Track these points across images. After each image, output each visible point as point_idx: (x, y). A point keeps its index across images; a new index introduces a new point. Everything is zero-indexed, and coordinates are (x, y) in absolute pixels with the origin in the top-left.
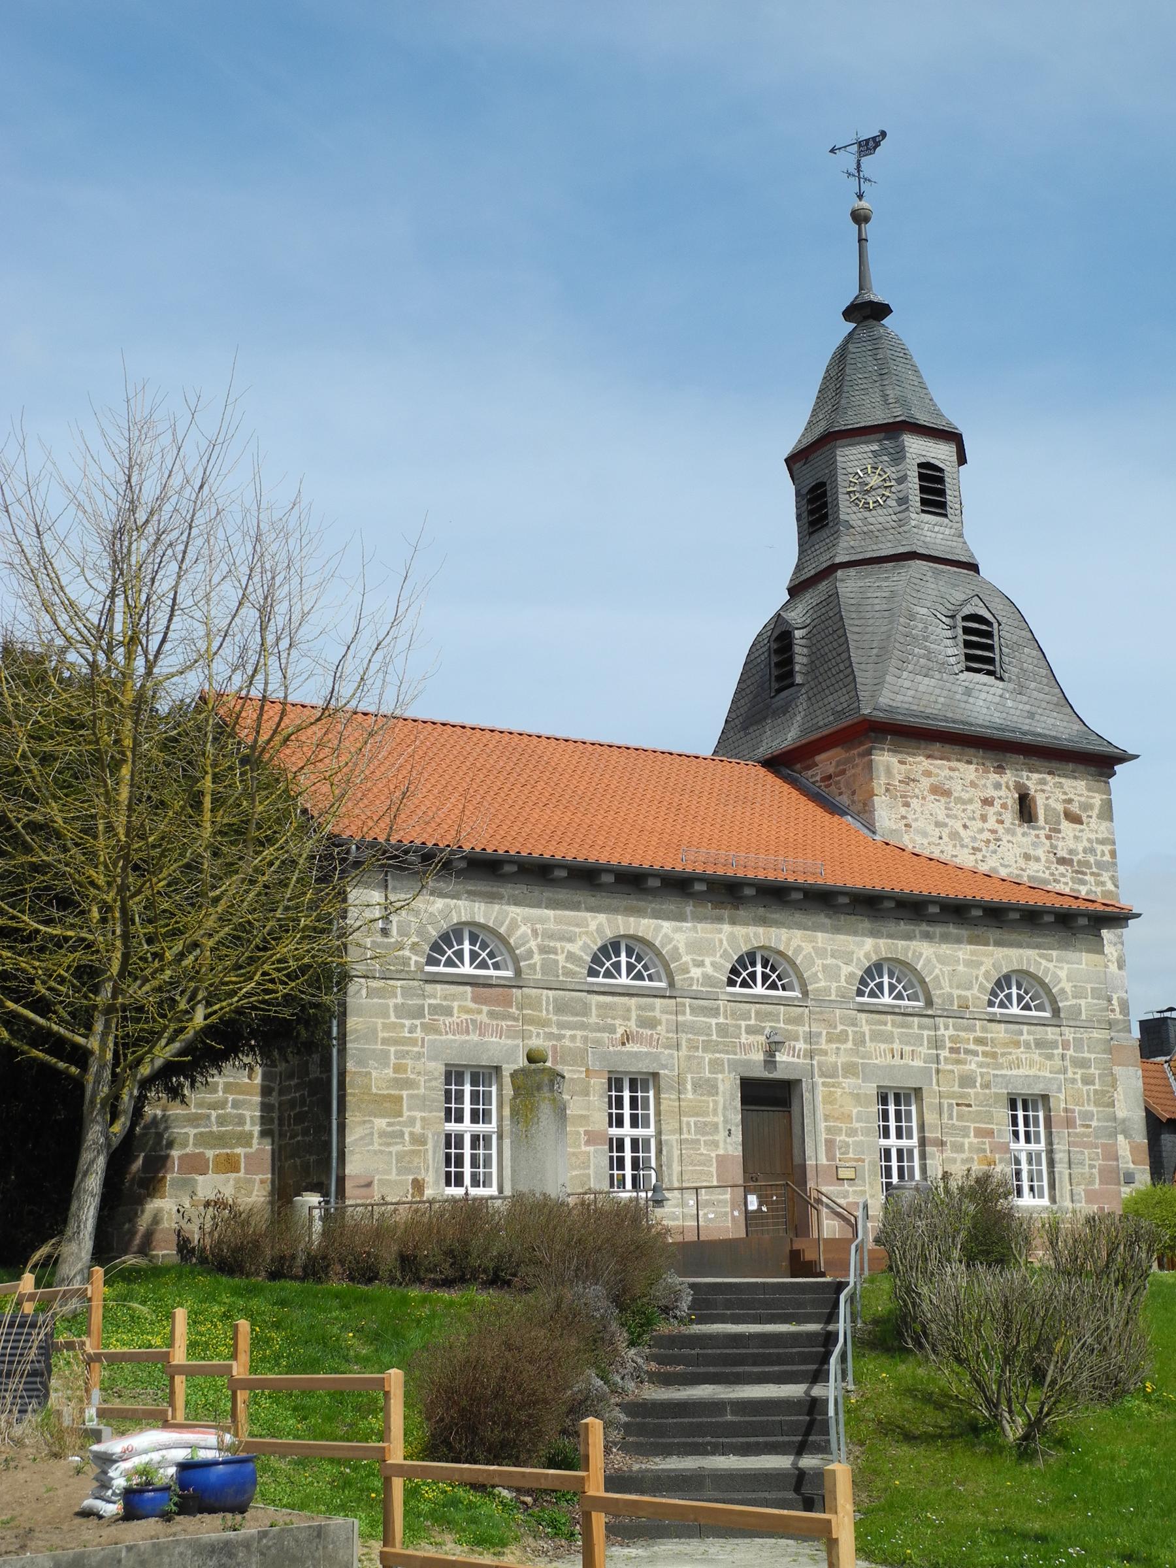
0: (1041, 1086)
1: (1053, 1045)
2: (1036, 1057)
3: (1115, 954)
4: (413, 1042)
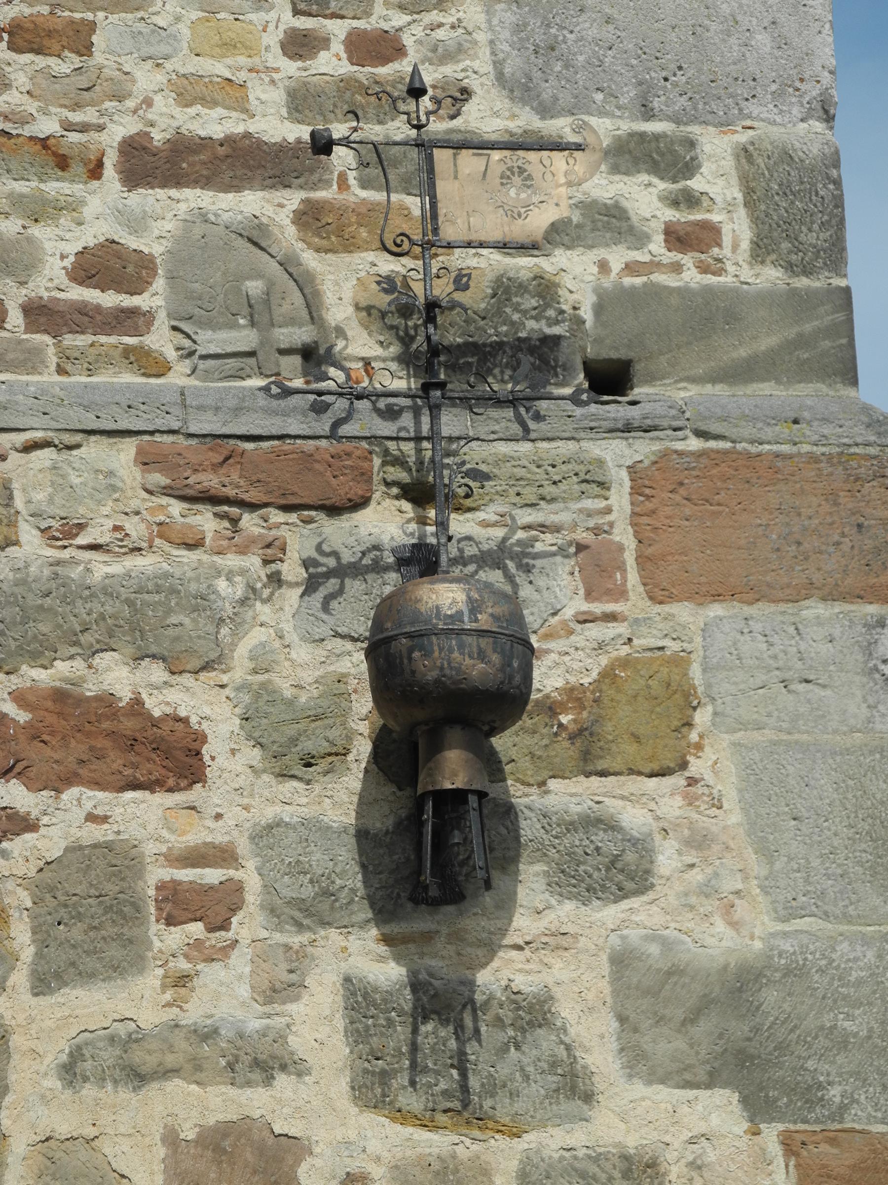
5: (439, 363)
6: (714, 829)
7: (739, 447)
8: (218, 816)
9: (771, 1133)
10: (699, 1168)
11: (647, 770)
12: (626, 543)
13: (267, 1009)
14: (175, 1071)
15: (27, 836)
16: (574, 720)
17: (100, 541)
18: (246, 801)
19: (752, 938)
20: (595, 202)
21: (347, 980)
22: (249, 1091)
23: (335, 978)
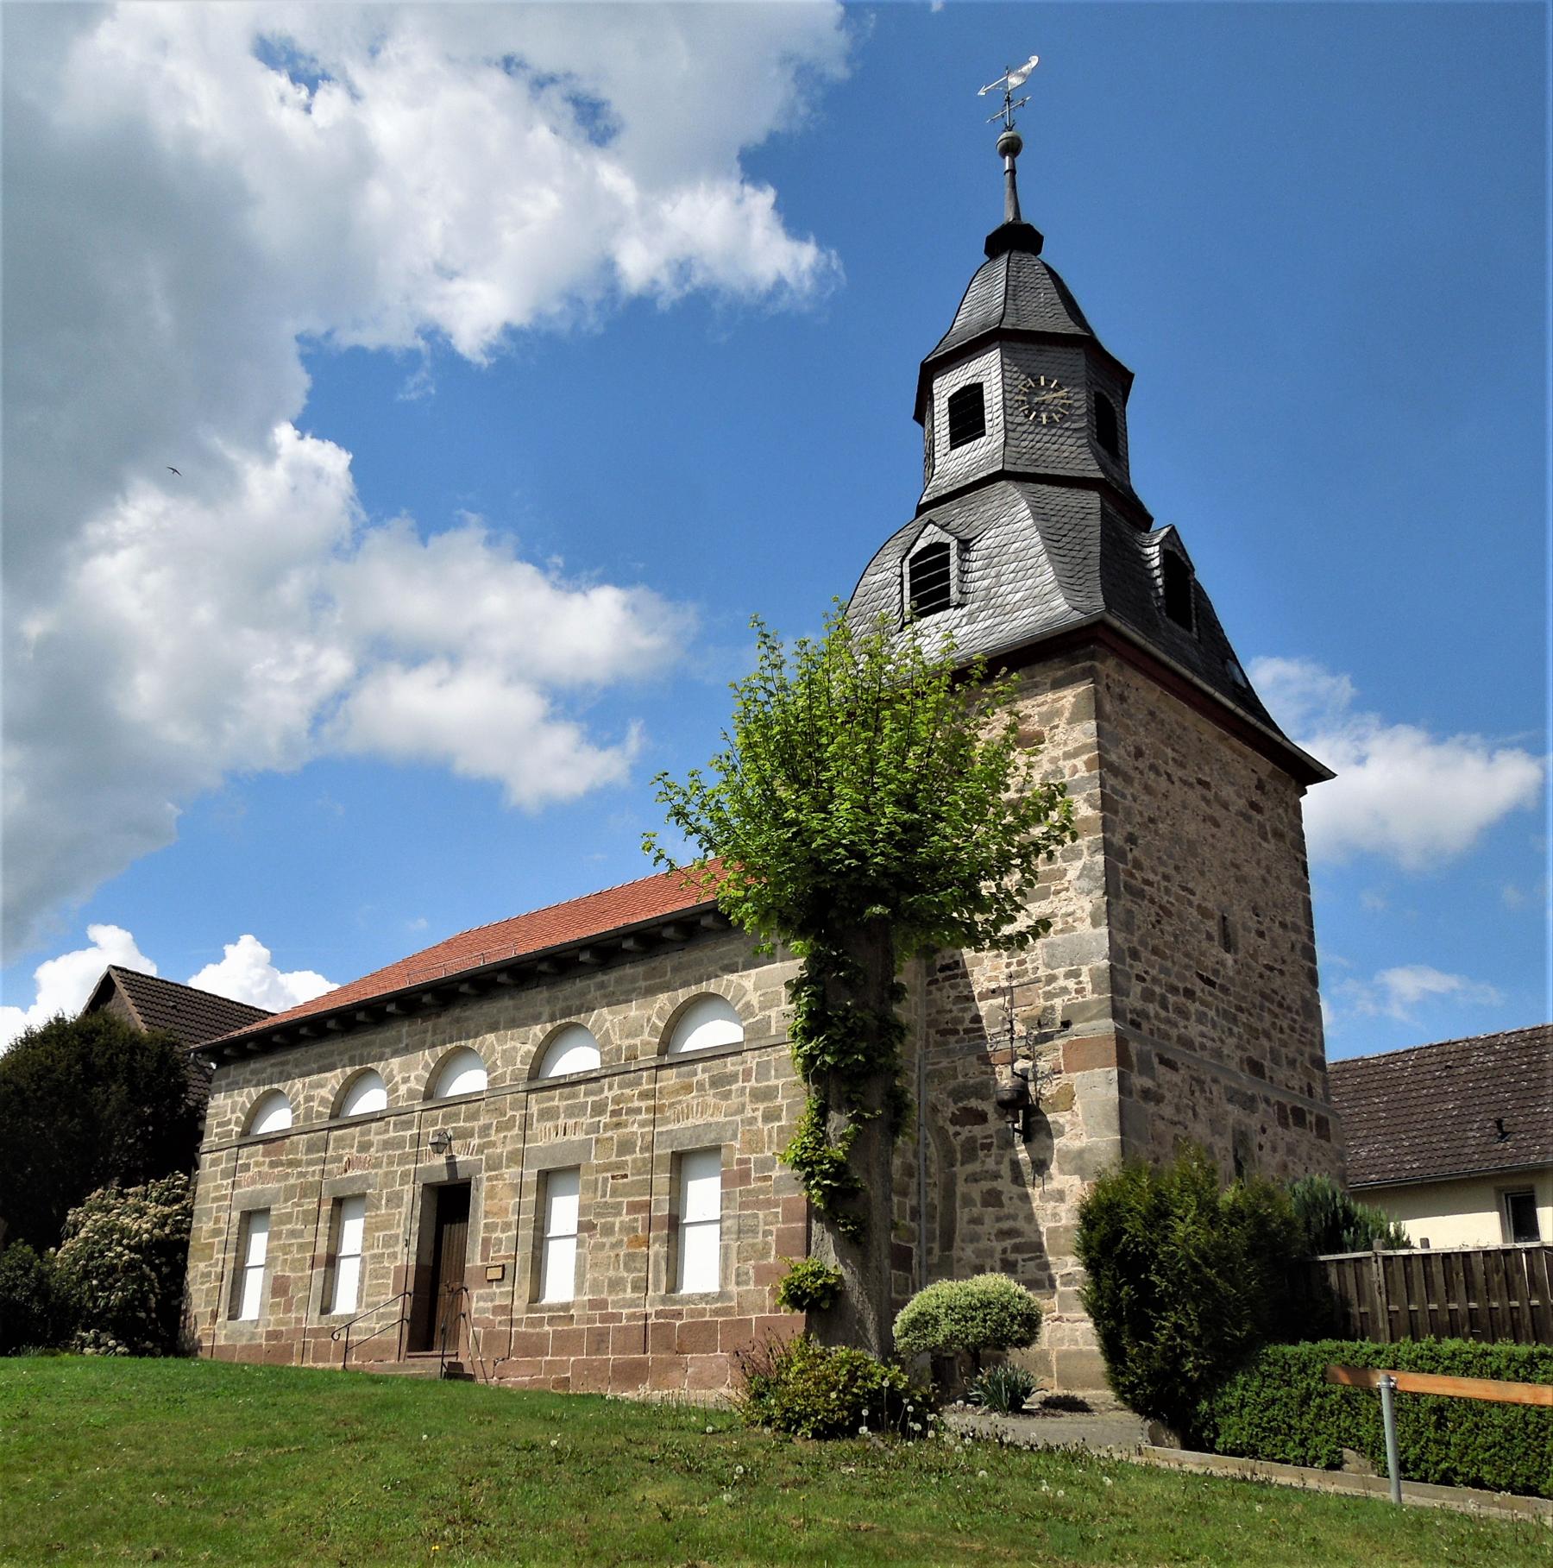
0: (712, 1136)
1: (733, 1078)
2: (711, 1100)
3: (1088, 907)
4: (224, 1197)
5: (95, 1306)
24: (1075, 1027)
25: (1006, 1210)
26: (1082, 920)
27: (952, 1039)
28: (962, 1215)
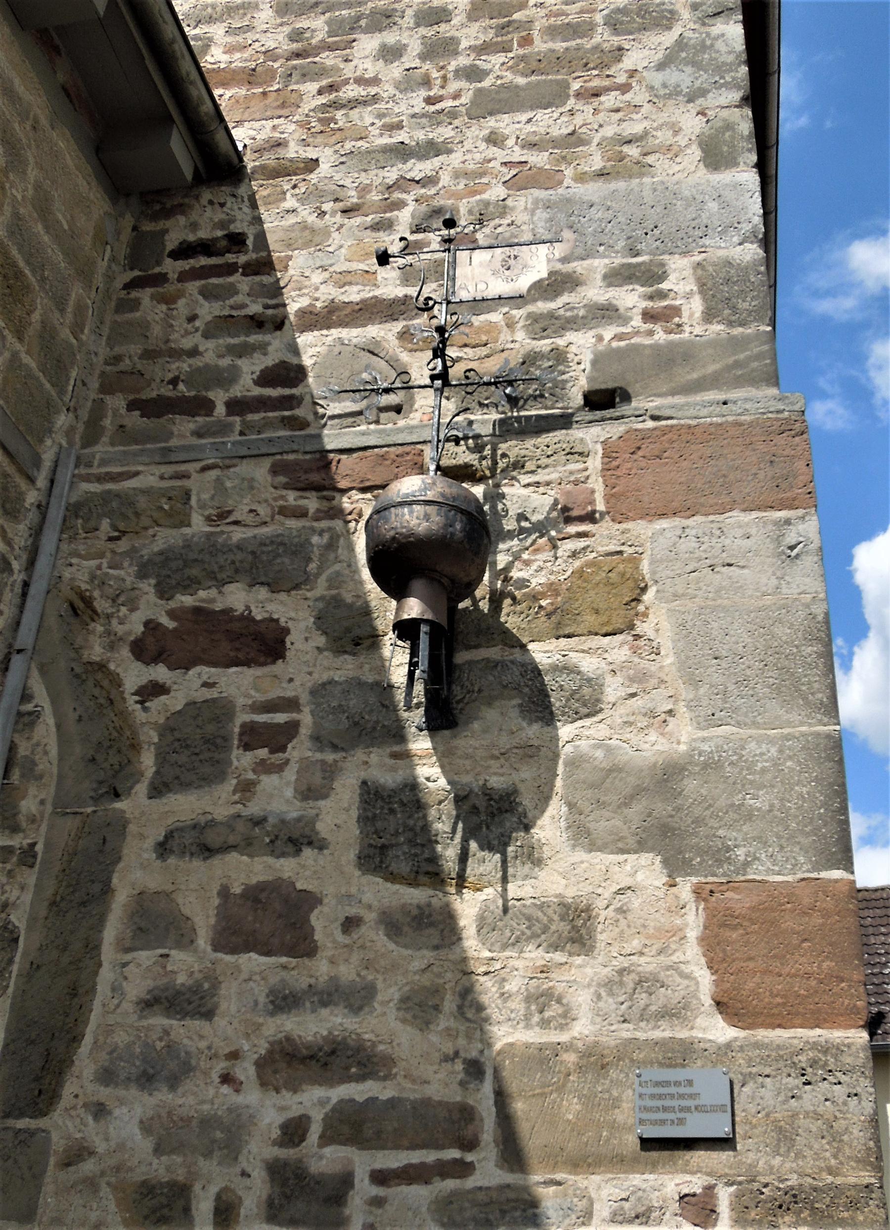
6: (653, 669)
7: (682, 422)
8: (291, 680)
9: (685, 888)
10: (625, 912)
11: (604, 631)
12: (597, 488)
13: (304, 804)
14: (234, 847)
15: (163, 698)
16: (552, 604)
17: (239, 519)
18: (311, 669)
19: (679, 743)
20: (596, 304)
21: (364, 783)
22: (282, 860)
23: (355, 782)
24: (638, 403)
25: (321, 969)
26: (673, 152)
27: (183, 428)
28: (123, 977)
